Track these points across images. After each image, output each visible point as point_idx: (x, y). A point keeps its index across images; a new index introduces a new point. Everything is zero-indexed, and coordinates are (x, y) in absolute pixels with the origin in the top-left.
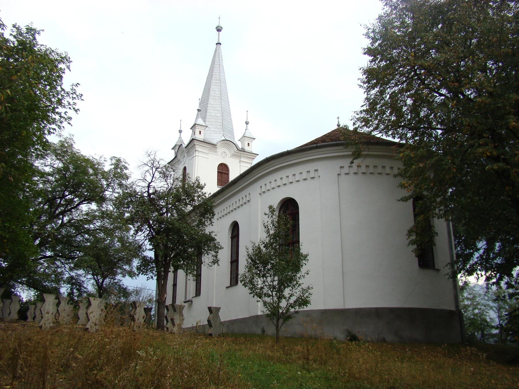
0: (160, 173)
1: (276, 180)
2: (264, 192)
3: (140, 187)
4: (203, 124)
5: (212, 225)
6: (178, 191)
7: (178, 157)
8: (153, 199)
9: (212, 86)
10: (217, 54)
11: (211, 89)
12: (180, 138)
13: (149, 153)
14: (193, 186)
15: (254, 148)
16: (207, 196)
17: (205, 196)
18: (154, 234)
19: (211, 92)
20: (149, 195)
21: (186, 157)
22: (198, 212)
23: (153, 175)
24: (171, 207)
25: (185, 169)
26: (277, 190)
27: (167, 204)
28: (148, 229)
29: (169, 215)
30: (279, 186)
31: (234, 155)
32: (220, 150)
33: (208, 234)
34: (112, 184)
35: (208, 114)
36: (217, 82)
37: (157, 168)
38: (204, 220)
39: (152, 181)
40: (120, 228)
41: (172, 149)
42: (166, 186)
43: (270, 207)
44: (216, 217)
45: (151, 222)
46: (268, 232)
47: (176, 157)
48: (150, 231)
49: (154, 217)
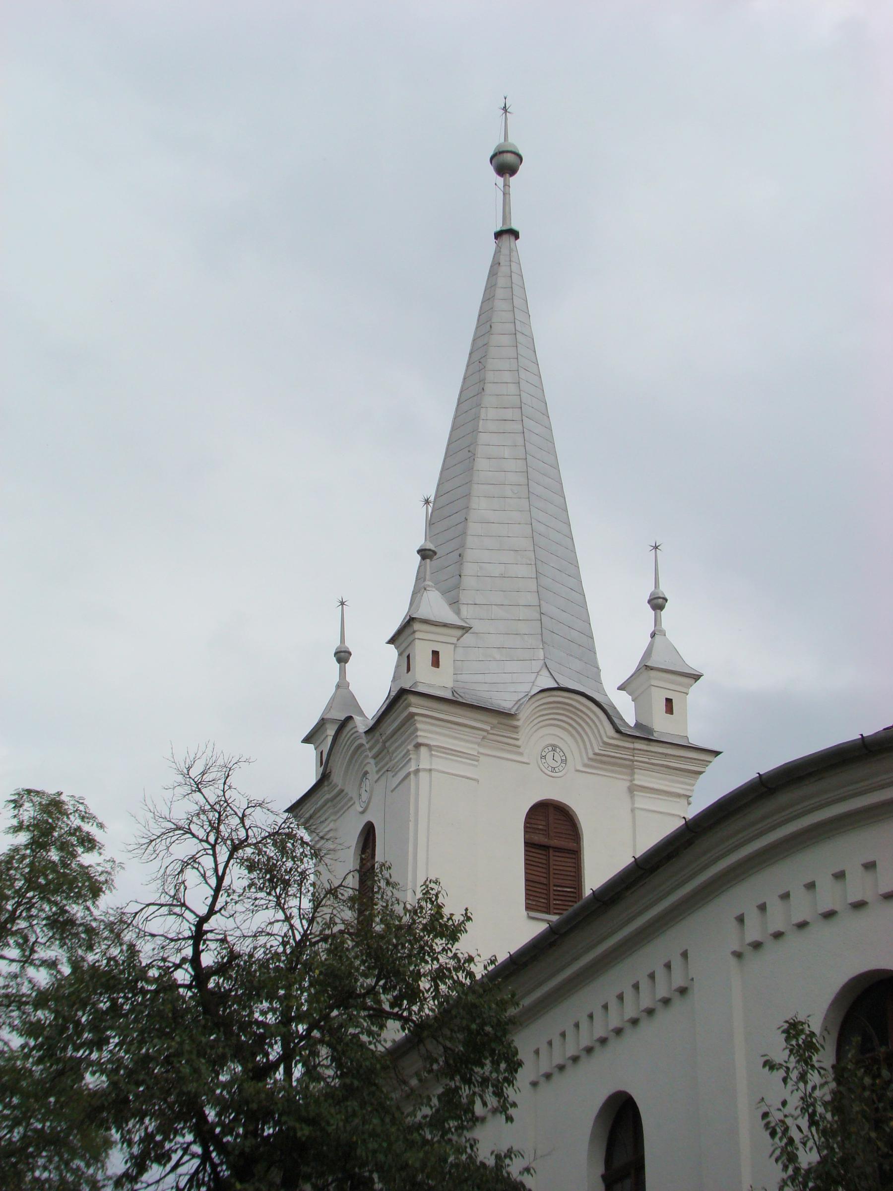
0: (251, 869)
1: (811, 886)
2: (757, 946)
3: (159, 941)
4: (449, 617)
5: (509, 1119)
6: (336, 950)
7: (337, 778)
8: (222, 997)
9: (483, 438)
10: (501, 282)
11: (481, 451)
12: (342, 685)
13: (195, 773)
14: (410, 928)
15: (696, 721)
16: (479, 971)
17: (471, 974)
18: (225, 1172)
19: (481, 464)
20: (201, 976)
21: (373, 776)
22: (437, 1051)
23: (220, 879)
24: (308, 1035)
25: (368, 834)
26: (822, 932)
27: (286, 1020)
28: (197, 1149)
29: (298, 1071)
30: (829, 915)
31: (601, 761)
32: (534, 736)
33: (491, 1162)
34: (22, 924)
35: (469, 569)
36: (509, 414)
37: (235, 848)
38: (465, 1091)
39: (212, 912)
40: (53, 1142)
41: (307, 740)
42: (281, 929)
43: (793, 1029)
44: (523, 1076)
45: (211, 1114)
46: (788, 1156)
47: (324, 779)
48: (205, 1157)
49: (224, 1085)
